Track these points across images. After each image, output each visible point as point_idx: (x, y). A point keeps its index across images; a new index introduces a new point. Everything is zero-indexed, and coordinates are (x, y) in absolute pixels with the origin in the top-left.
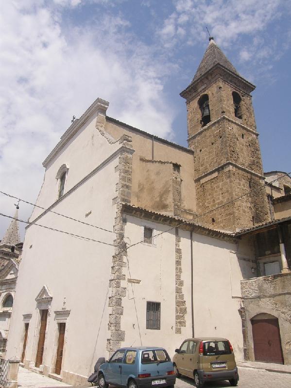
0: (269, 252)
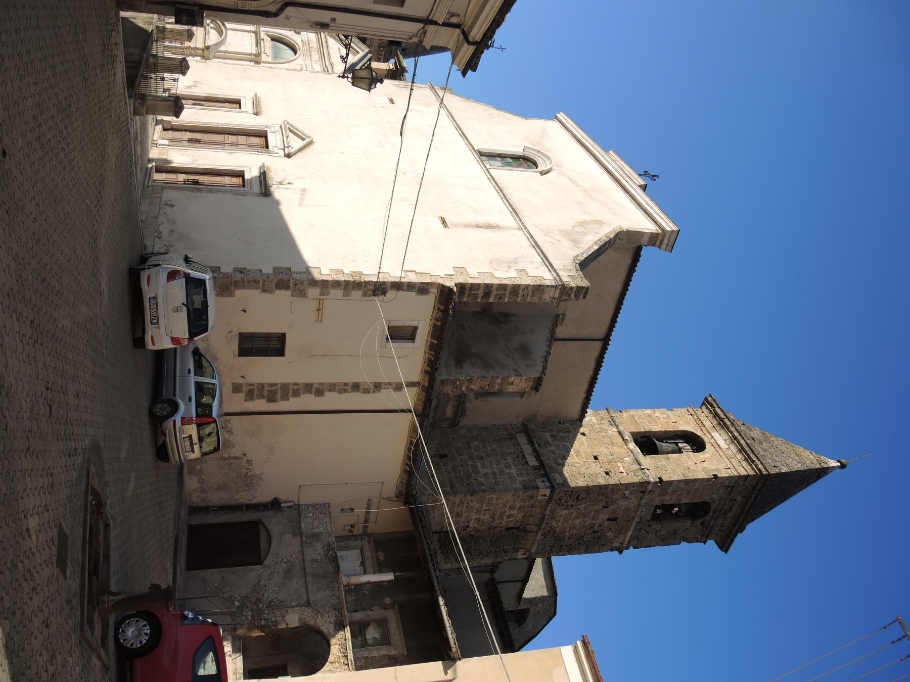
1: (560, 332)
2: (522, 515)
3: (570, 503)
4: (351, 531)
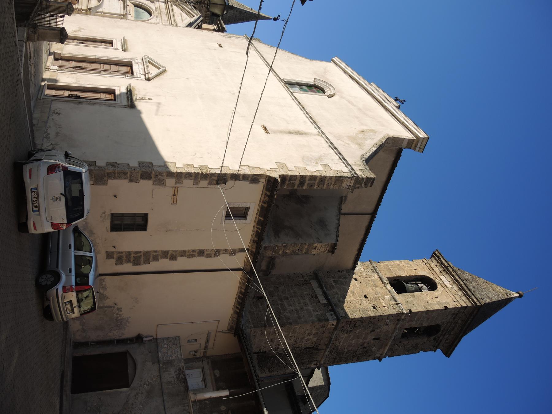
0: (218, 375)
1: (345, 209)
2: (316, 339)
3: (349, 329)
4: (195, 355)
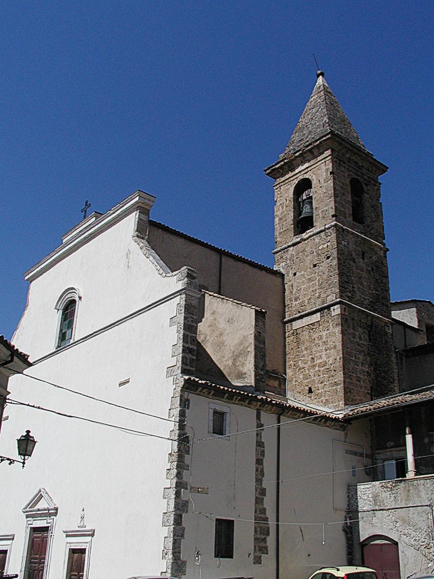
0: (392, 444)
3: (351, 289)
